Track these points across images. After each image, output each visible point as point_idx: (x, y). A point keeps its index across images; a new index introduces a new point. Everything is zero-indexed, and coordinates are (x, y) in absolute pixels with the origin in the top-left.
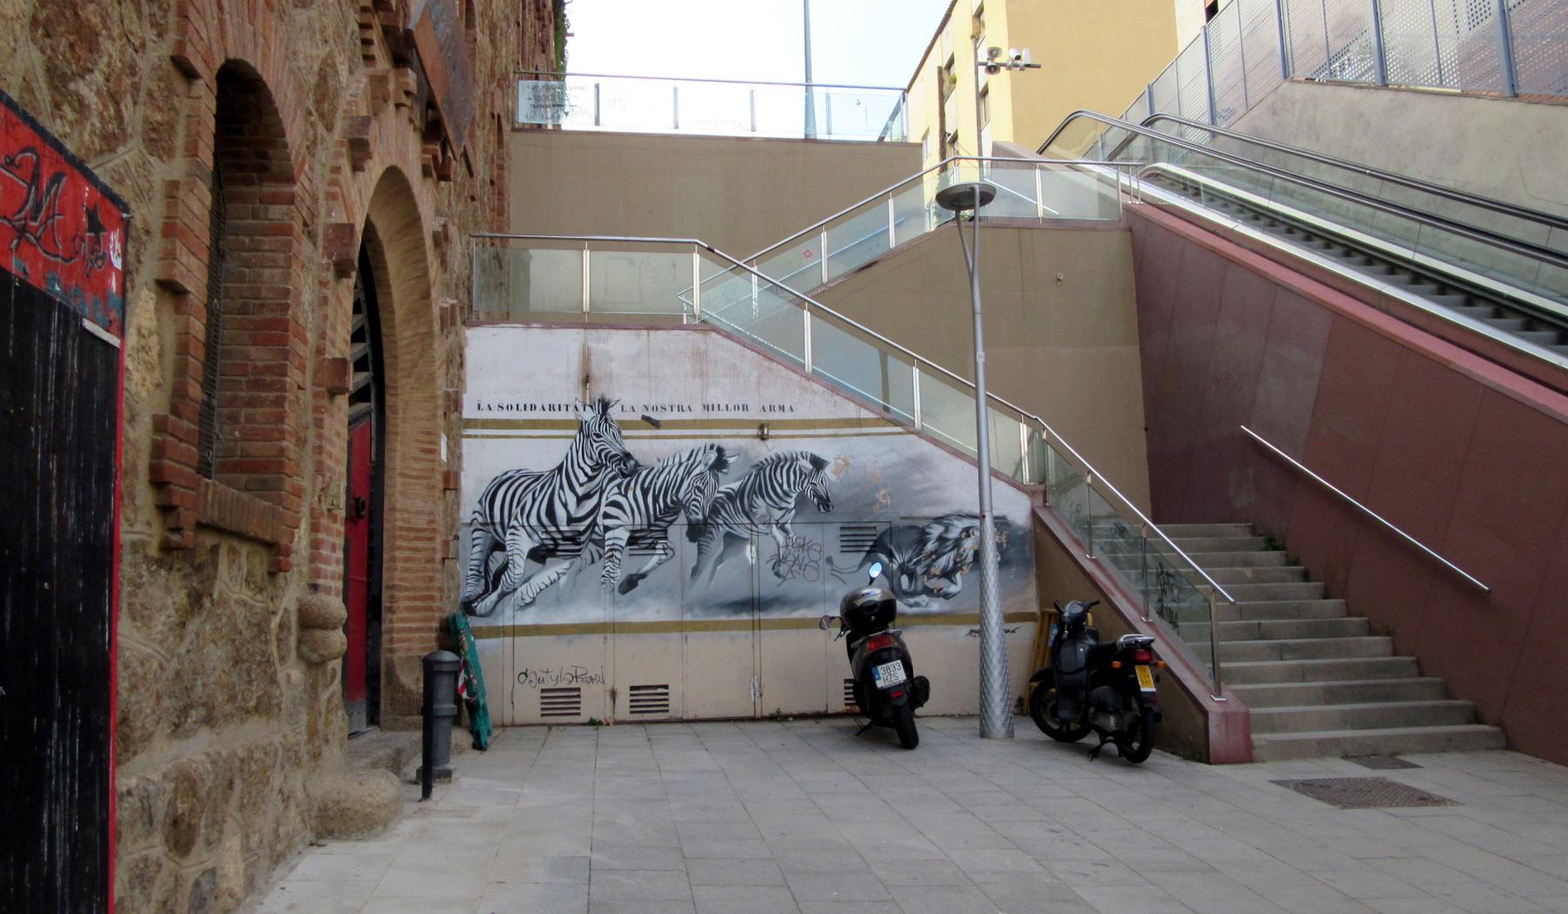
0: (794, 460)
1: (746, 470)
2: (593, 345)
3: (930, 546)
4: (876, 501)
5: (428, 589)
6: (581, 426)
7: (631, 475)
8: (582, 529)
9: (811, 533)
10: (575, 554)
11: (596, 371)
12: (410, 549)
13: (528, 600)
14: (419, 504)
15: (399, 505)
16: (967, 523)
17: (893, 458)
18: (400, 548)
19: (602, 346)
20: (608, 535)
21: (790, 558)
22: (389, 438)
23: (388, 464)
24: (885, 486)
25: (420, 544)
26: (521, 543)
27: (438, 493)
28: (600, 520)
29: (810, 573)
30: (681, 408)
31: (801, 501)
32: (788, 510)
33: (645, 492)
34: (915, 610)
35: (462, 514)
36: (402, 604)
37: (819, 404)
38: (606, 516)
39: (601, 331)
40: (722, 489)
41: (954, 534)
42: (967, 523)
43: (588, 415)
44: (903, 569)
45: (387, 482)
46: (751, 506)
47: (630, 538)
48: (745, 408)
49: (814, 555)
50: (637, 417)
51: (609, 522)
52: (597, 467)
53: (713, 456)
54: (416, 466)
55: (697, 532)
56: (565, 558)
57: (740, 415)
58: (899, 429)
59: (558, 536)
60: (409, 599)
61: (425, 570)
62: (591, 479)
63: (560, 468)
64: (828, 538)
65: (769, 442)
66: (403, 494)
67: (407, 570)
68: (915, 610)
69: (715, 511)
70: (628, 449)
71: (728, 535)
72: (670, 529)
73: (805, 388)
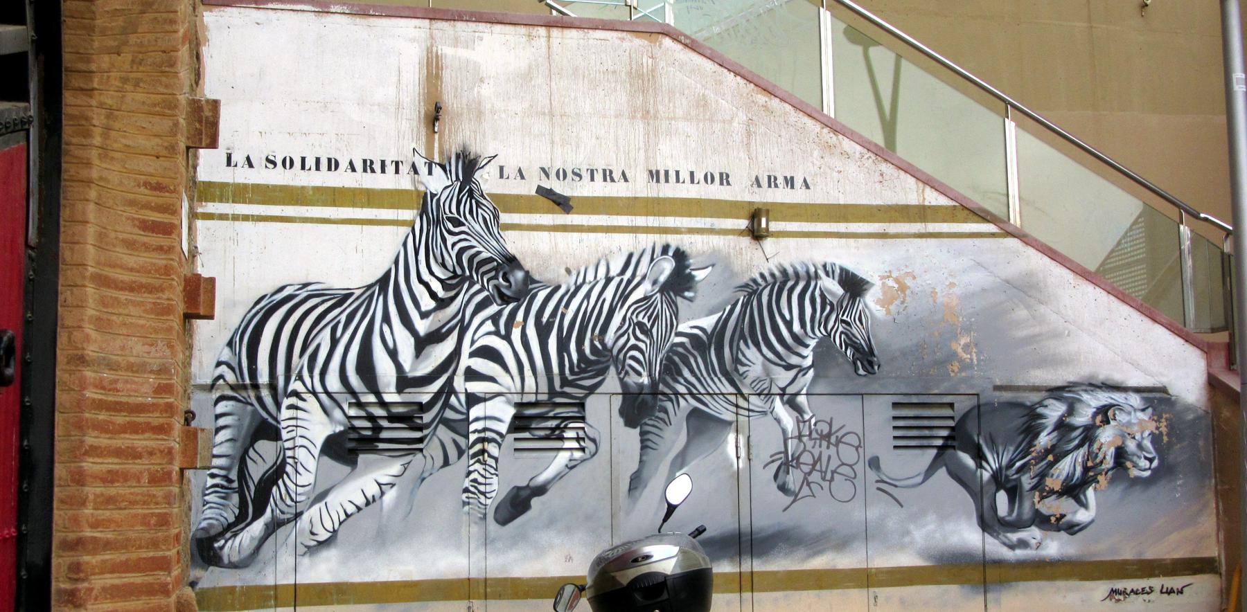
0: (811, 277)
1: (728, 294)
2: (447, 51)
3: (1044, 440)
4: (953, 356)
5: (155, 544)
6: (424, 203)
7: (517, 298)
8: (425, 399)
9: (844, 414)
10: (412, 447)
11: (450, 101)
12: (118, 453)
13: (324, 535)
14: (138, 349)
15: (91, 351)
16: (1103, 398)
17: (978, 279)
18: (95, 451)
19: (462, 53)
20: (476, 411)
21: (806, 458)
22: (70, 191)
23: (65, 252)
24: (967, 330)
25: (141, 442)
26: (311, 426)
27: (175, 322)
28: (459, 383)
29: (842, 487)
30: (608, 176)
31: (824, 352)
32: (803, 371)
33: (543, 332)
34: (1020, 553)
35: (194, 368)
36: (99, 582)
37: (853, 179)
38: (471, 375)
39: (460, 25)
40: (684, 327)
41: (1082, 418)
42: (1103, 398)
43: (437, 182)
44: (999, 480)
45: (65, 295)
46: (736, 361)
47: (516, 417)
48: (725, 179)
49: (848, 454)
50: (527, 188)
51: (476, 387)
52: (454, 283)
53: (668, 266)
54: (132, 260)
55: (639, 408)
56: (394, 454)
57: (716, 192)
58: (990, 228)
59: (379, 412)
60: (115, 568)
61: (149, 500)
62: (442, 304)
63: (383, 282)
64: (873, 421)
65: (768, 243)
66: (102, 324)
67: (110, 501)
68: (1020, 553)
69: (671, 369)
70: (512, 249)
71: (695, 414)
72: (591, 402)
73: (829, 147)
